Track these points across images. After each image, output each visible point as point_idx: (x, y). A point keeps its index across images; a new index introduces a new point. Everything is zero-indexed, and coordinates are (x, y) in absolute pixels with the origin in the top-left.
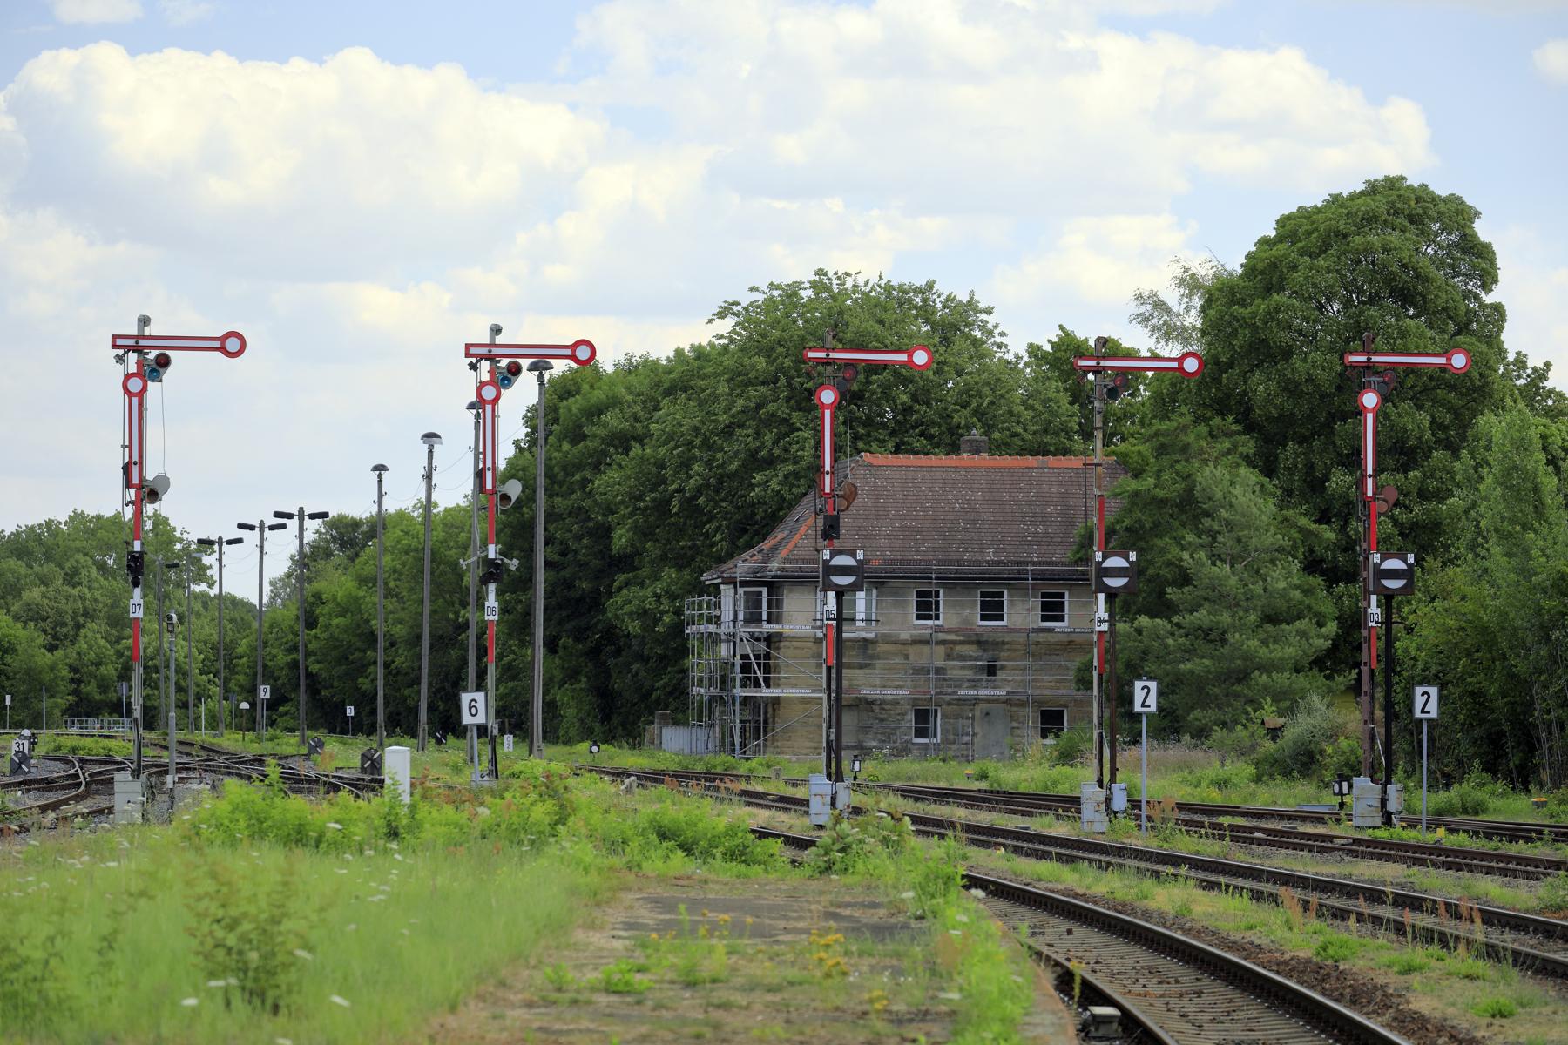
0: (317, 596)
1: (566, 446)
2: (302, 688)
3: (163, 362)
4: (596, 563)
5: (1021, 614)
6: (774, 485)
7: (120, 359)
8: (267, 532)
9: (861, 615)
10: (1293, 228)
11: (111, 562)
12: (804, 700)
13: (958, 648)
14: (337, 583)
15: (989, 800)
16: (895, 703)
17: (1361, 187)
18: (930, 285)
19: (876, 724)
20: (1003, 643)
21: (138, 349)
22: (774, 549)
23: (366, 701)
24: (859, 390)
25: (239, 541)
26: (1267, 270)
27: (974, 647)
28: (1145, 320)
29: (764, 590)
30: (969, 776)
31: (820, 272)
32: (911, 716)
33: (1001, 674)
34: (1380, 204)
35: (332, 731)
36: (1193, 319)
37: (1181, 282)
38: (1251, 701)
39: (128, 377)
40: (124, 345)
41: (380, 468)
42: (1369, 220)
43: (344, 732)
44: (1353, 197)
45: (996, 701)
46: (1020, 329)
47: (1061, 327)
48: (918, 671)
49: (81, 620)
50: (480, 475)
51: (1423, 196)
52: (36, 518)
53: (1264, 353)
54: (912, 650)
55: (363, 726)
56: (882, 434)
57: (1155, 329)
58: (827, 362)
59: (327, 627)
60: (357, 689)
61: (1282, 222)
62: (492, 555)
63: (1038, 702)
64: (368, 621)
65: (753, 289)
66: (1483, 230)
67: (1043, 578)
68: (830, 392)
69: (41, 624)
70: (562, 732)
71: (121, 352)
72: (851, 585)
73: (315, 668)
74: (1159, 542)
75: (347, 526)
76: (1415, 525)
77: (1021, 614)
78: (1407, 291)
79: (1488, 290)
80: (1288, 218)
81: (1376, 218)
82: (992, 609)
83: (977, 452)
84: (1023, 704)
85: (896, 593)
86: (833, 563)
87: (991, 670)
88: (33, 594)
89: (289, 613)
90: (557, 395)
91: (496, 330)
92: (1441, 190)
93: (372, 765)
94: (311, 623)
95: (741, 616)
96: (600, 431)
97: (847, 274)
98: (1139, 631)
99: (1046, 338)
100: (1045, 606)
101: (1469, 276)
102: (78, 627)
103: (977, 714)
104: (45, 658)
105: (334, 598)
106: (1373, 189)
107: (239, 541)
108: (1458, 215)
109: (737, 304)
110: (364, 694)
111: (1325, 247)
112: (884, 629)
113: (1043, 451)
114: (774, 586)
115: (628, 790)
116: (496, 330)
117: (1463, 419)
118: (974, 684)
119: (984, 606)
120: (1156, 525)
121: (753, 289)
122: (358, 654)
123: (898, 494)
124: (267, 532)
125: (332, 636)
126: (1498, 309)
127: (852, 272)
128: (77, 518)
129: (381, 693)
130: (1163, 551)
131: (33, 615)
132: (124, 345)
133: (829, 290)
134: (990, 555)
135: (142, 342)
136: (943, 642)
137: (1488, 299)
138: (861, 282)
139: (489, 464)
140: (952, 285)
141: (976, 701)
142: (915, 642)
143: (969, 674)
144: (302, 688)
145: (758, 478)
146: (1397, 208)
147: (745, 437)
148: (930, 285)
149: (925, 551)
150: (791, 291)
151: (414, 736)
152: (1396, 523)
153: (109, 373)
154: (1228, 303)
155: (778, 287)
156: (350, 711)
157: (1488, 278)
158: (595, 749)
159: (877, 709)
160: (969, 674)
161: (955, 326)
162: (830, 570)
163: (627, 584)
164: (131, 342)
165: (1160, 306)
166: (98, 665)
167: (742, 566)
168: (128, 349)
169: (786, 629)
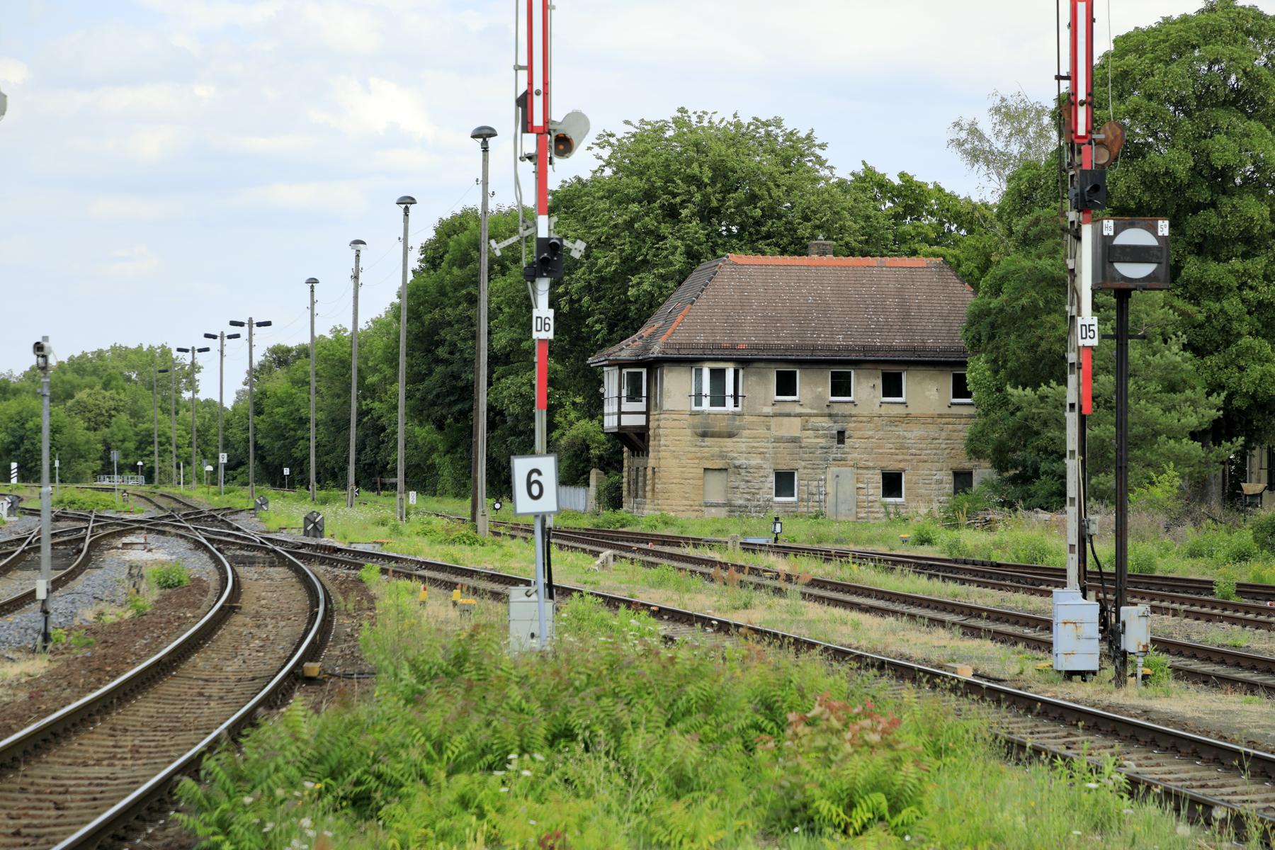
0: (264, 393)
1: (455, 271)
2: (251, 456)
6: (646, 286)
8: (226, 341)
11: (134, 376)
13: (813, 419)
14: (279, 383)
15: (958, 570)
19: (743, 485)
20: (851, 416)
22: (652, 336)
23: (300, 465)
25: (207, 350)
27: (826, 419)
28: (960, 144)
29: (644, 371)
30: (905, 541)
31: (682, 110)
32: (772, 478)
35: (273, 485)
37: (997, 110)
41: (312, 281)
43: (282, 486)
47: (864, 163)
48: (778, 440)
49: (113, 412)
52: (91, 347)
54: (773, 421)
55: (298, 481)
57: (965, 152)
59: (270, 415)
60: (291, 456)
62: (543, 232)
63: (882, 469)
64: (298, 410)
65: (627, 122)
68: (711, 198)
69: (88, 415)
70: (439, 486)
72: (1148, 278)
73: (261, 442)
75: (283, 352)
77: (866, 389)
81: (1221, 31)
83: (824, 254)
86: (1119, 241)
88: (82, 395)
89: (248, 405)
93: (315, 528)
94: (259, 412)
95: (624, 393)
97: (705, 113)
98: (1043, 398)
102: (111, 416)
103: (829, 477)
105: (276, 394)
107: (207, 350)
109: (611, 135)
110: (295, 459)
114: (654, 365)
115: (604, 565)
121: (627, 122)
122: (292, 433)
123: (747, 290)
124: (226, 341)
125: (274, 422)
127: (710, 112)
129: (313, 459)
130: (1054, 327)
131: (82, 409)
133: (689, 125)
134: (840, 340)
136: (800, 415)
138: (716, 120)
139: (538, 85)
140: (797, 122)
144: (251, 456)
145: (635, 280)
147: (625, 243)
149: (785, 337)
150: (659, 129)
155: (648, 123)
156: (286, 471)
158: (497, 506)
159: (743, 472)
165: (974, 131)
166: (123, 441)
167: (627, 349)
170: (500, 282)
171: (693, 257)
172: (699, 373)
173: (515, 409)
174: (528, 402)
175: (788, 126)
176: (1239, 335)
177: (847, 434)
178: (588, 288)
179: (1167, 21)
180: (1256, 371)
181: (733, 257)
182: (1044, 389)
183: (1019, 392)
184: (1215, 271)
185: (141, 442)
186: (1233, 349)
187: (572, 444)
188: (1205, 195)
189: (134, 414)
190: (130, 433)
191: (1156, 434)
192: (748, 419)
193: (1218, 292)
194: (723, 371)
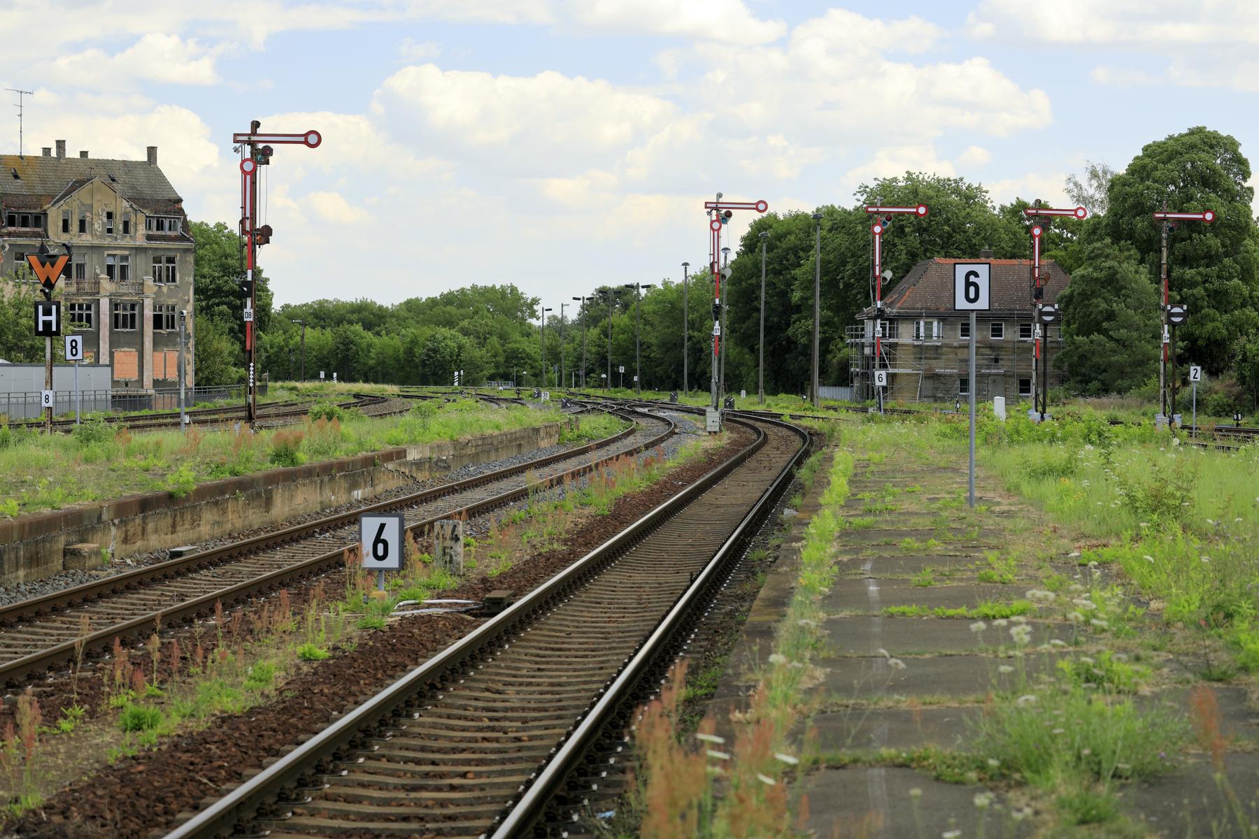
3: (729, 215)
4: (781, 309)
5: (1010, 334)
7: (709, 213)
9: (935, 334)
10: (1151, 151)
12: (908, 375)
16: (951, 376)
17: (1185, 131)
18: (961, 179)
21: (717, 209)
24: (898, 228)
26: (1139, 170)
33: (1001, 362)
34: (1196, 139)
36: (1100, 195)
38: (1145, 375)
39: (243, 161)
40: (712, 207)
42: (1193, 147)
44: (1181, 136)
45: (998, 375)
46: (1000, 195)
50: (712, 265)
51: (1215, 135)
52: (455, 287)
53: (1140, 209)
56: (938, 248)
58: (1165, 219)
61: (1145, 149)
66: (1244, 151)
67: (1021, 317)
71: (238, 145)
74: (1095, 301)
76: (1216, 292)
77: (1010, 334)
78: (1208, 181)
79: (1245, 179)
80: (1149, 146)
82: (997, 331)
84: (1011, 376)
85: (952, 324)
87: (996, 360)
90: (759, 227)
91: (720, 196)
92: (1223, 133)
96: (784, 246)
98: (1092, 342)
99: (1009, 201)
100: (1022, 330)
101: (1236, 175)
104: (477, 353)
106: (1192, 132)
108: (1230, 145)
111: (1170, 159)
112: (947, 341)
113: (1013, 256)
116: (720, 196)
117: (1236, 243)
118: (988, 367)
119: (993, 330)
120: (1093, 292)
126: (1251, 190)
128: (474, 287)
130: (1097, 306)
132: (712, 207)
135: (254, 138)
137: (1246, 185)
141: (990, 375)
142: (960, 347)
143: (985, 362)
146: (1204, 141)
148: (961, 179)
151: (709, 390)
152: (1206, 290)
153: (704, 220)
154: (1118, 189)
157: (1246, 175)
160: (985, 362)
161: (970, 197)
162: (1041, 313)
163: (799, 320)
164: (246, 138)
168: (713, 208)
169: (900, 341)
170: (771, 255)
171: (913, 256)
172: (918, 323)
173: (803, 341)
174: (810, 334)
175: (967, 181)
176: (1202, 308)
177: (161, 377)
178: (853, 274)
179: (1171, 138)
180: (1210, 326)
181: (937, 259)
182: (1092, 337)
183: (1080, 338)
184: (1189, 273)
185: (507, 358)
186: (1199, 315)
187: (839, 363)
188: (1185, 233)
189: (501, 337)
190: (501, 351)
191: (1149, 359)
192: (945, 349)
193: (1192, 284)
194: (931, 323)
